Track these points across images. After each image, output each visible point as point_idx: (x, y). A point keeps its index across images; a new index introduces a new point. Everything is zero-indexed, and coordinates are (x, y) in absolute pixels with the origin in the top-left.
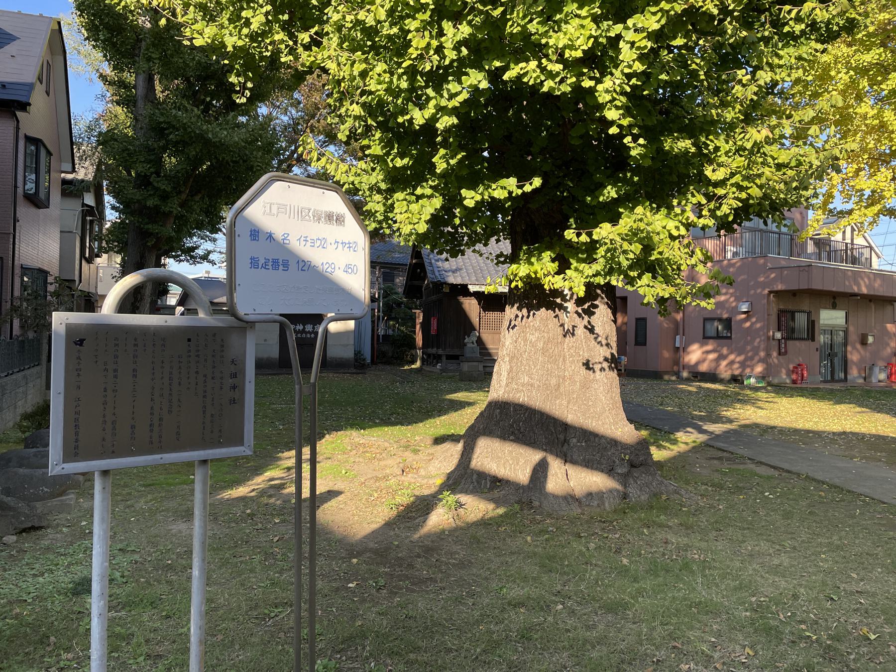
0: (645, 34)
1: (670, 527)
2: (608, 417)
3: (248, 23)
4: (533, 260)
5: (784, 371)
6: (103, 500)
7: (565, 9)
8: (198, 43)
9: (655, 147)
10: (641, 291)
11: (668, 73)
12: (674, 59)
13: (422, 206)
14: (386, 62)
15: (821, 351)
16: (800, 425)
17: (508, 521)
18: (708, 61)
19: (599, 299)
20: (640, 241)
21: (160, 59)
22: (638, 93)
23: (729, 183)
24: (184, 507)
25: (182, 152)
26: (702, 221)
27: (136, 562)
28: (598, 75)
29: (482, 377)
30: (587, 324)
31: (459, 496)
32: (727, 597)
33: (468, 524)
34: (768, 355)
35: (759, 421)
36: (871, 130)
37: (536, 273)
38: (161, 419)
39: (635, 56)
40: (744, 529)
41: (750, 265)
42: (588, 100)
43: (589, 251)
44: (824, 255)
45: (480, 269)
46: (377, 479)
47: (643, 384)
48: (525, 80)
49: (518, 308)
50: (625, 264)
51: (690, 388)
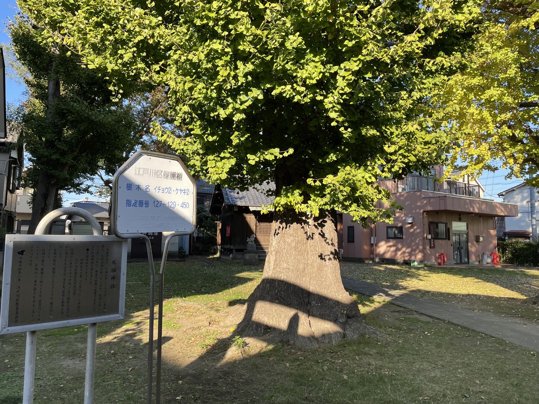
0: (351, 72)
1: (371, 355)
2: (334, 288)
3: (121, 57)
4: (289, 195)
5: (433, 257)
6: (32, 349)
7: (306, 57)
8: (91, 67)
9: (357, 133)
10: (352, 214)
11: (363, 93)
12: (367, 85)
13: (224, 163)
14: (204, 83)
15: (454, 246)
16: (444, 290)
17: (275, 354)
18: (385, 87)
19: (327, 217)
20: (349, 185)
21: (64, 72)
22: (347, 103)
23: (398, 153)
24: (71, 350)
25: (76, 127)
26: (384, 175)
27: (41, 386)
28: (325, 93)
29: (259, 262)
30: (320, 232)
31: (245, 338)
32: (405, 397)
33: (250, 356)
34: (424, 248)
35: (420, 288)
36: (476, 122)
37: (291, 202)
38: (68, 299)
39: (345, 84)
40: (414, 355)
41: (412, 195)
42: (319, 106)
43: (321, 191)
44: (453, 190)
45: (257, 199)
46: (194, 329)
47: (353, 266)
48: (284, 95)
49: (280, 222)
50: (341, 198)
51: (380, 268)
